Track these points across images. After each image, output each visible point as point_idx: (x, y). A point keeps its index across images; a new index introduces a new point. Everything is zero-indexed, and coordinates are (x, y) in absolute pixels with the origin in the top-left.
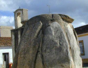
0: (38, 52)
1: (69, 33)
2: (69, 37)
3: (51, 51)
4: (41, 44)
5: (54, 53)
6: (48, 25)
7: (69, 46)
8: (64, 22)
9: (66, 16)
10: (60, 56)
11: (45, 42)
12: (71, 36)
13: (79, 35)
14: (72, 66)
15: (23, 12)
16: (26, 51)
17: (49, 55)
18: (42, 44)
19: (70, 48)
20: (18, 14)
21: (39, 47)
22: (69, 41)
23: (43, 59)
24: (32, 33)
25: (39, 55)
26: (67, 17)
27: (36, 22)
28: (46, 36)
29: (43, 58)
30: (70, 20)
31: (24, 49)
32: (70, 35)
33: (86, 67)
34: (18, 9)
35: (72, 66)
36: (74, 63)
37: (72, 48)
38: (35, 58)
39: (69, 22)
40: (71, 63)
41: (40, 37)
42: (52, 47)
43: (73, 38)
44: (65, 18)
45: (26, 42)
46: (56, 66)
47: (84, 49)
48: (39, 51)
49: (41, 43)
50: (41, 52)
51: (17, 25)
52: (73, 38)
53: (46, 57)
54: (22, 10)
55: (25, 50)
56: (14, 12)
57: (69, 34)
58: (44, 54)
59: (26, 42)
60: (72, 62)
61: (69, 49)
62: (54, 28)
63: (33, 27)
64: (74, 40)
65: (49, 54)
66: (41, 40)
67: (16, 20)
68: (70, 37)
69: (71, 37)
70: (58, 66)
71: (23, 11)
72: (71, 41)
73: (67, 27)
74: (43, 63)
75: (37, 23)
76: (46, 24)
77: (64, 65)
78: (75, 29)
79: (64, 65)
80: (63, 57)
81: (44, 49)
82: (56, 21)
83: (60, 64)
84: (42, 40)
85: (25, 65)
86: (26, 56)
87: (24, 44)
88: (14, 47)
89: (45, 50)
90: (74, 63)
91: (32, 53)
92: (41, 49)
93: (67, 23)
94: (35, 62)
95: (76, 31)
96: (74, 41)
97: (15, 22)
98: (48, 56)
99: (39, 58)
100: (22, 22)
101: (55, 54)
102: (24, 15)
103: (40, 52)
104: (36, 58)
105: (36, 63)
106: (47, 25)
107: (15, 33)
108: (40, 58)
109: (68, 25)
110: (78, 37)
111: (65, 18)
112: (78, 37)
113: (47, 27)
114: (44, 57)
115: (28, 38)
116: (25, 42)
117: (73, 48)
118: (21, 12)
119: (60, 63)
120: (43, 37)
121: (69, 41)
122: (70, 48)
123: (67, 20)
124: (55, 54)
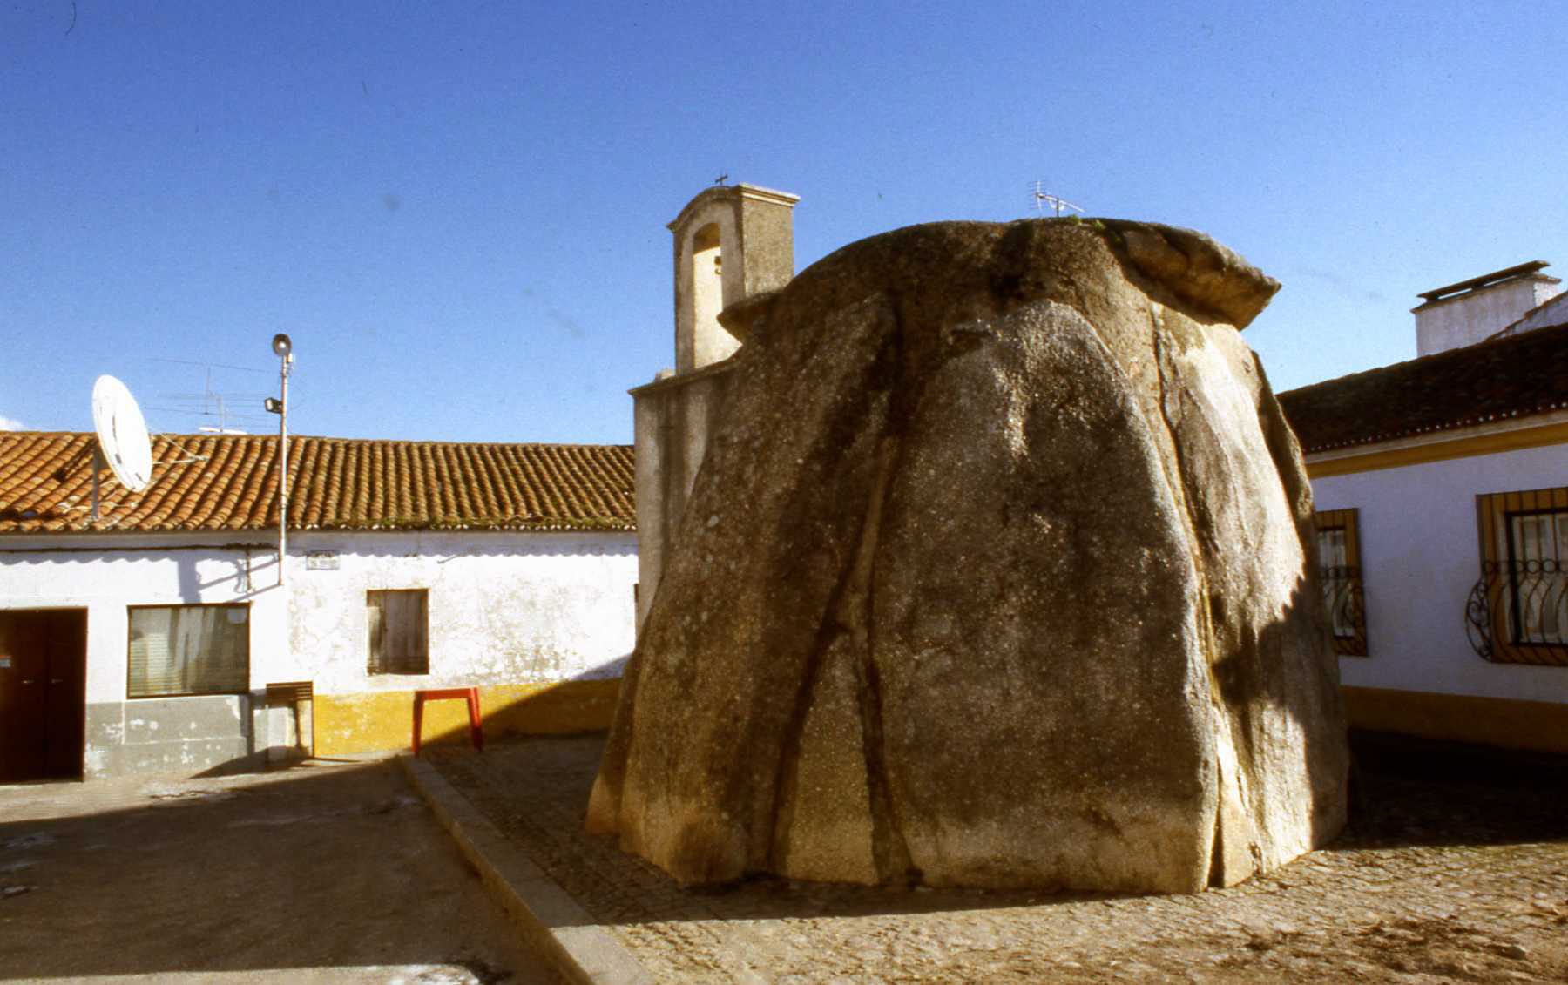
0: (831, 628)
1: (1208, 429)
2: (1202, 476)
3: (972, 635)
4: (866, 550)
5: (1013, 658)
6: (959, 335)
7: (1195, 584)
8: (1158, 308)
9: (1180, 243)
10: (1079, 705)
11: (913, 523)
12: (1231, 465)
13: (1325, 457)
14: (1219, 823)
15: (746, 214)
16: (704, 616)
17: (943, 678)
18: (879, 544)
19: (1217, 604)
20: (704, 240)
21: (846, 575)
22: (1203, 524)
23: (878, 721)
24: (777, 424)
25: (840, 674)
26: (1198, 257)
27: (834, 306)
28: (924, 454)
29: (878, 705)
30: (1232, 289)
31: (691, 592)
32: (1219, 458)
33: (1266, 305)
34: (708, 192)
35: (1219, 823)
36: (1256, 783)
37: (1231, 614)
38: (791, 694)
39: (1209, 311)
40: (1211, 792)
41: (868, 465)
42: (988, 586)
43: (1249, 492)
44: (1175, 265)
45: (713, 521)
46: (1019, 811)
47: (1368, 598)
48: (844, 628)
49: (871, 532)
50: (862, 636)
51: (693, 341)
52: (1249, 492)
53: (910, 692)
54: (732, 197)
55: (699, 599)
56: (671, 226)
57: (1203, 439)
58: (891, 654)
59: (713, 521)
60: (1230, 779)
61: (1191, 619)
62: (1030, 365)
63: (795, 357)
64: (1263, 515)
65: (949, 661)
66: (877, 500)
67: (684, 300)
68: (1222, 477)
69: (1236, 482)
70: (1047, 812)
71: (748, 209)
72: (1232, 523)
73: (1193, 368)
74: (875, 767)
75: (841, 315)
76: (937, 330)
77: (1117, 809)
78: (1287, 398)
79: (1117, 809)
80: (1114, 707)
81: (901, 606)
82: (1060, 297)
83: (1063, 801)
84: (887, 497)
85: (682, 768)
86: (701, 664)
87: (701, 531)
88: (653, 543)
89: (910, 621)
90: (1256, 783)
91: (757, 638)
92: (869, 604)
93: (1185, 321)
94: (790, 740)
95: (1290, 420)
96: (1261, 529)
97: (677, 321)
98: (934, 693)
99: (831, 706)
100: (733, 317)
101: (1016, 679)
102: (748, 248)
103: (851, 632)
104: (805, 697)
105: (797, 753)
106: (945, 330)
107: (668, 420)
108: (848, 703)
109: (1200, 343)
110: (1311, 476)
111: (1175, 265)
112: (1314, 472)
113: (954, 352)
114: (890, 698)
115: (740, 480)
116: (706, 519)
117: (1242, 611)
118: (722, 215)
119: (1071, 782)
120: (903, 462)
121: (1203, 524)
122: (1217, 604)
123: (1195, 291)
124: (1014, 670)
